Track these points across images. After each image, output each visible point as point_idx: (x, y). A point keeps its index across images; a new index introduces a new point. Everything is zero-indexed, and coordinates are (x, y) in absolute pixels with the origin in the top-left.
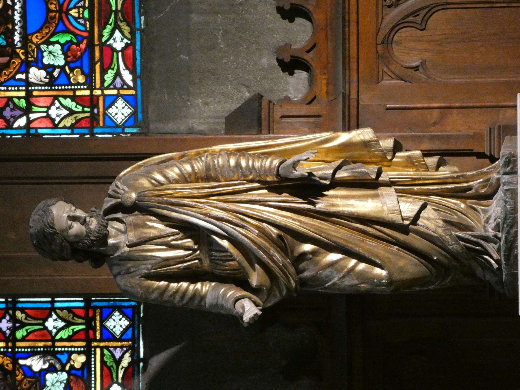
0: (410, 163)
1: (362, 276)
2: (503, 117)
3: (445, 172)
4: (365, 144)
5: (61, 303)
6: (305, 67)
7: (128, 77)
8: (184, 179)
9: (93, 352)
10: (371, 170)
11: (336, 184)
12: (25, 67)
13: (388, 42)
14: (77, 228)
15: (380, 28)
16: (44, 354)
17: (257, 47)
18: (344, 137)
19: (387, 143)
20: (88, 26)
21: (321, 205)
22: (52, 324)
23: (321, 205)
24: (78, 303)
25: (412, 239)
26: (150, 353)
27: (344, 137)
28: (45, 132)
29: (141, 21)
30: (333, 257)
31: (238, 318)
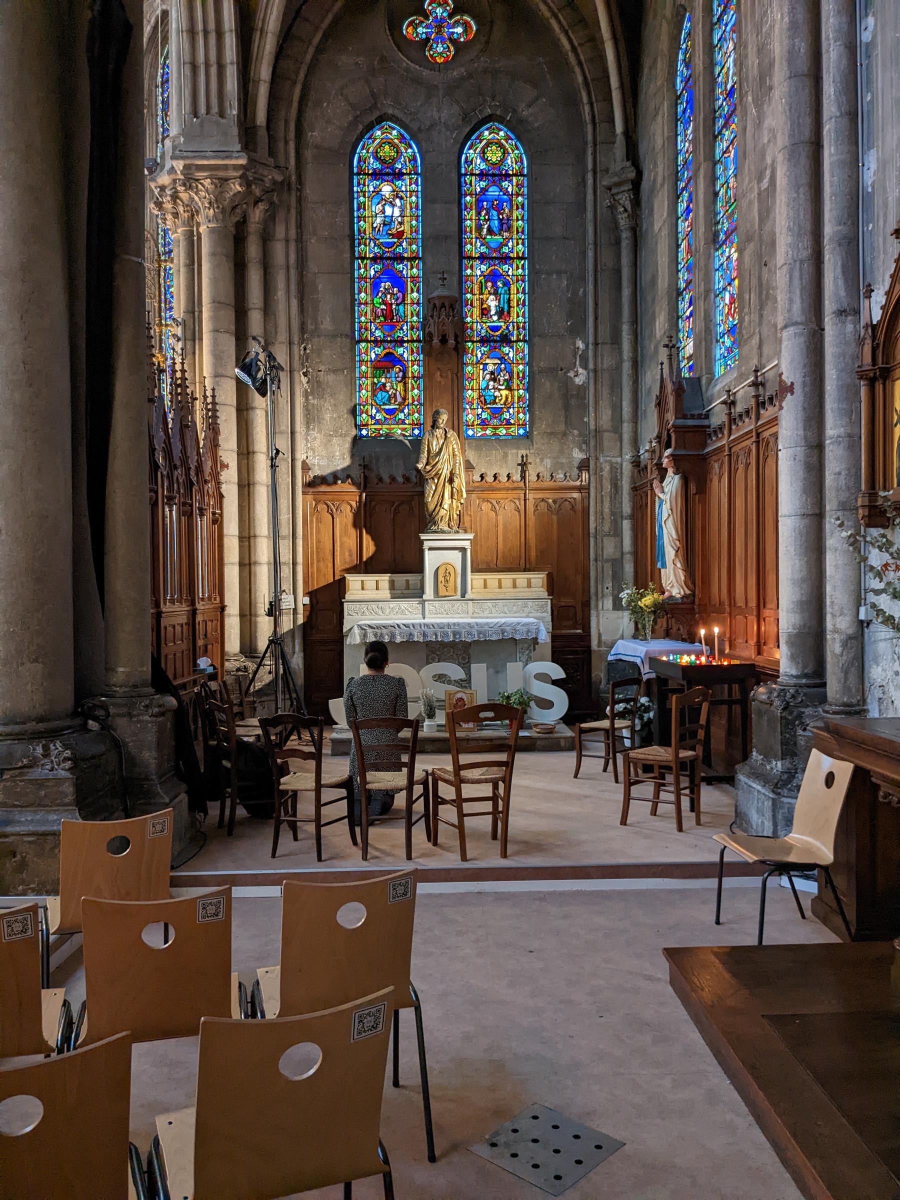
0: (457, 507)
1: (429, 495)
2: (469, 530)
3: (455, 516)
4: (462, 496)
5: (422, 417)
6: (482, 480)
7: (479, 434)
8: (453, 449)
9: (146, 103)
10: (456, 497)
11: (452, 488)
12: (482, 408)
13: (488, 501)
14: (441, 421)
15: (214, 403)
16: (409, 414)
17: (18, 857)
18: (464, 490)
19: (462, 501)
20: (526, 352)
21: (447, 484)
22: (416, 415)
23: (447, 484)
24: (422, 422)
25: (438, 507)
26: (409, 441)
27: (464, 490)
28: (465, 414)
29: (493, 438)
30: (434, 487)
31: (417, 462)
